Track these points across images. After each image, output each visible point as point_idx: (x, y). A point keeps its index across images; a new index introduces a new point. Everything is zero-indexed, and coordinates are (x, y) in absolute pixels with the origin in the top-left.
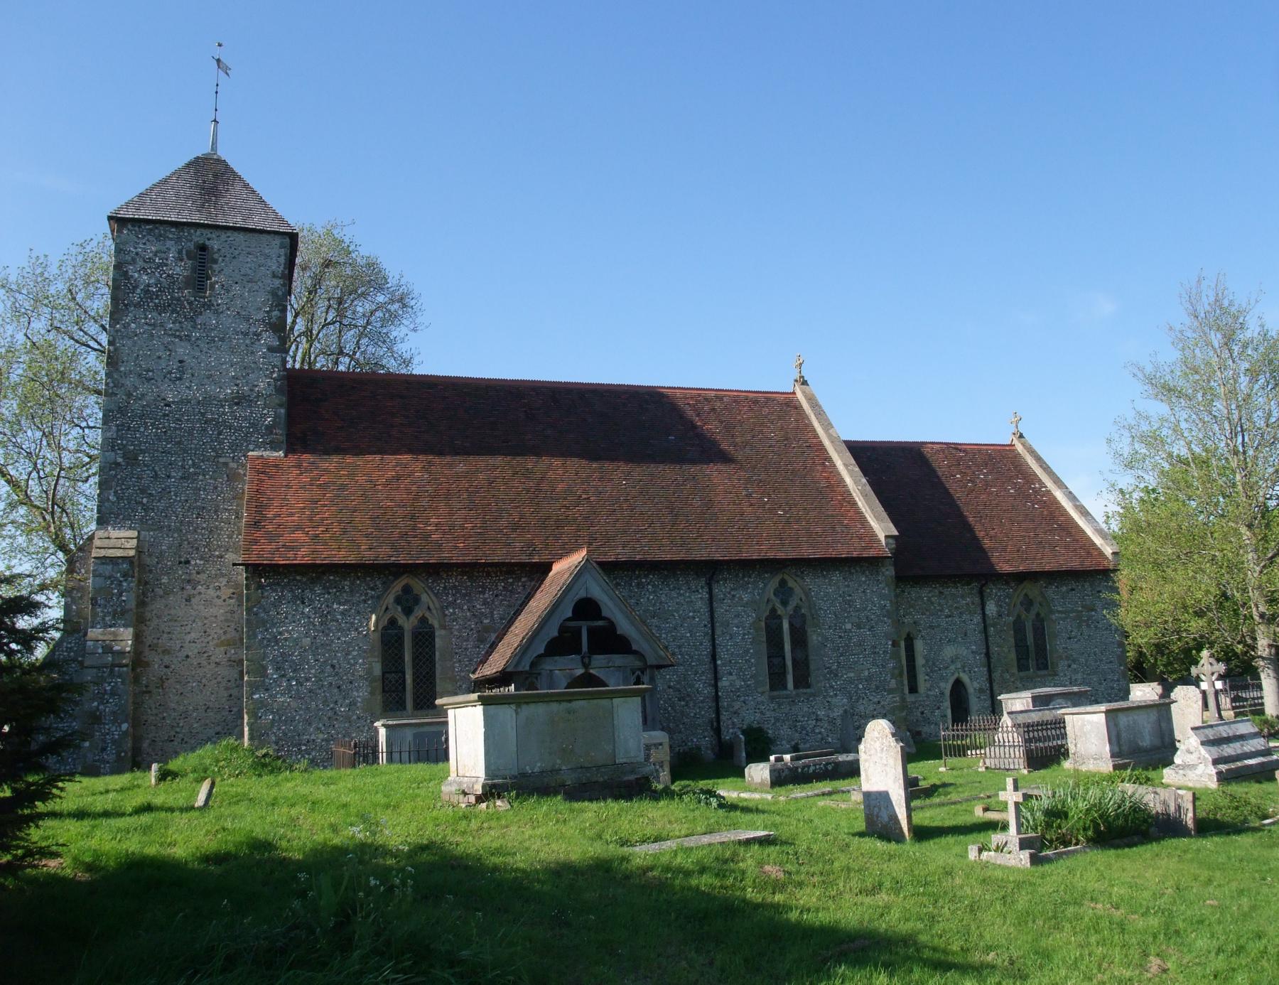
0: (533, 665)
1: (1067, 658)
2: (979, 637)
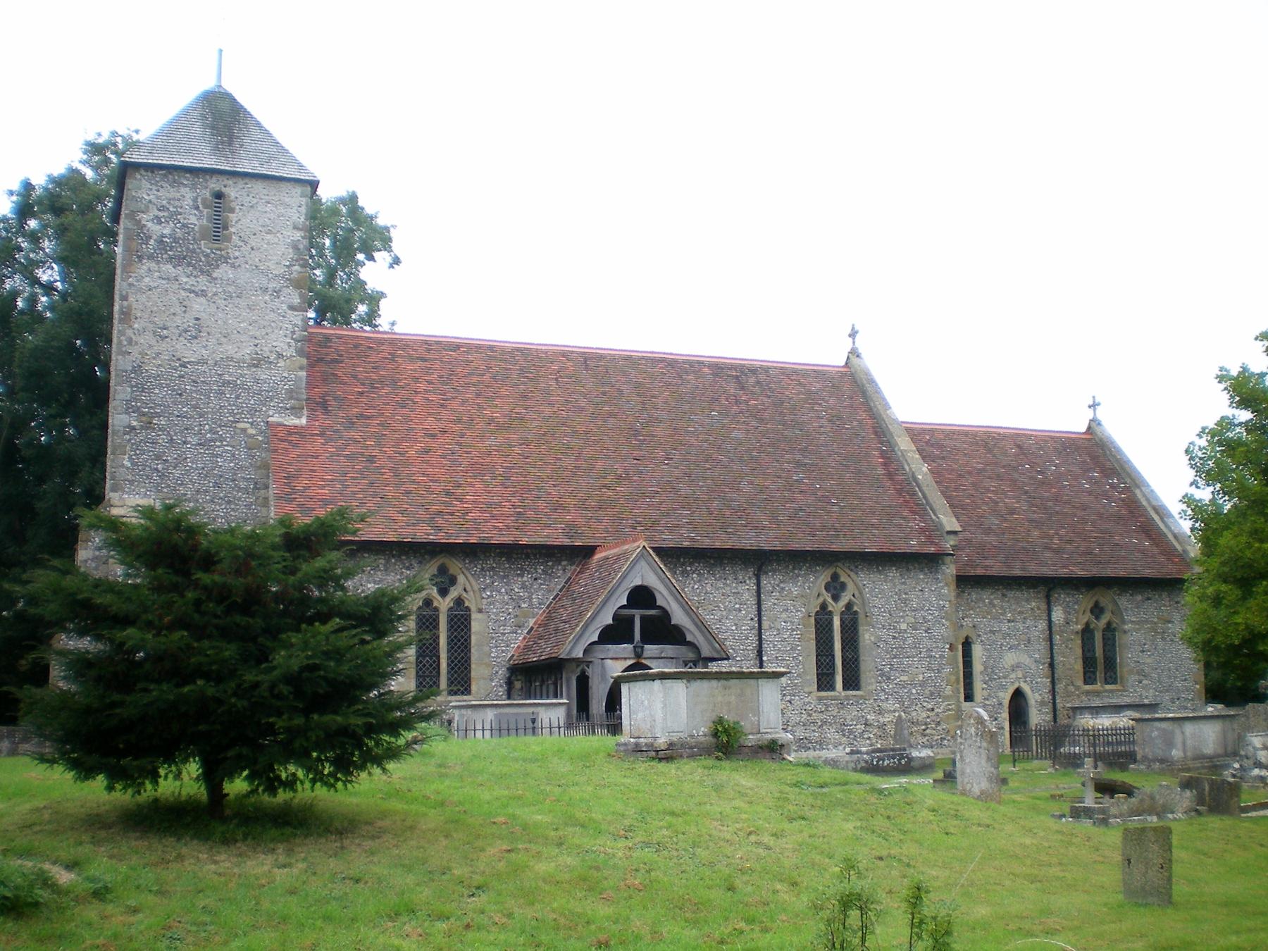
0: (586, 651)
1: (1138, 673)
2: (1043, 646)
